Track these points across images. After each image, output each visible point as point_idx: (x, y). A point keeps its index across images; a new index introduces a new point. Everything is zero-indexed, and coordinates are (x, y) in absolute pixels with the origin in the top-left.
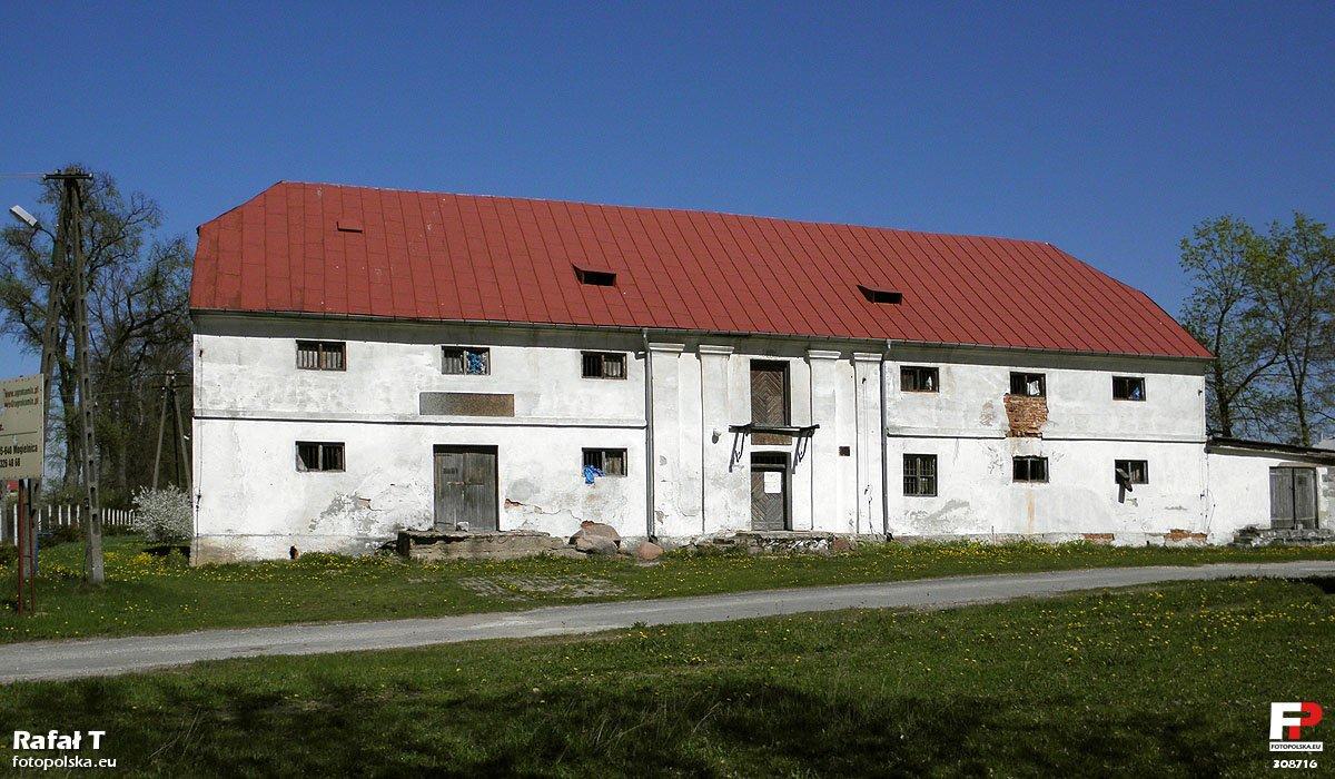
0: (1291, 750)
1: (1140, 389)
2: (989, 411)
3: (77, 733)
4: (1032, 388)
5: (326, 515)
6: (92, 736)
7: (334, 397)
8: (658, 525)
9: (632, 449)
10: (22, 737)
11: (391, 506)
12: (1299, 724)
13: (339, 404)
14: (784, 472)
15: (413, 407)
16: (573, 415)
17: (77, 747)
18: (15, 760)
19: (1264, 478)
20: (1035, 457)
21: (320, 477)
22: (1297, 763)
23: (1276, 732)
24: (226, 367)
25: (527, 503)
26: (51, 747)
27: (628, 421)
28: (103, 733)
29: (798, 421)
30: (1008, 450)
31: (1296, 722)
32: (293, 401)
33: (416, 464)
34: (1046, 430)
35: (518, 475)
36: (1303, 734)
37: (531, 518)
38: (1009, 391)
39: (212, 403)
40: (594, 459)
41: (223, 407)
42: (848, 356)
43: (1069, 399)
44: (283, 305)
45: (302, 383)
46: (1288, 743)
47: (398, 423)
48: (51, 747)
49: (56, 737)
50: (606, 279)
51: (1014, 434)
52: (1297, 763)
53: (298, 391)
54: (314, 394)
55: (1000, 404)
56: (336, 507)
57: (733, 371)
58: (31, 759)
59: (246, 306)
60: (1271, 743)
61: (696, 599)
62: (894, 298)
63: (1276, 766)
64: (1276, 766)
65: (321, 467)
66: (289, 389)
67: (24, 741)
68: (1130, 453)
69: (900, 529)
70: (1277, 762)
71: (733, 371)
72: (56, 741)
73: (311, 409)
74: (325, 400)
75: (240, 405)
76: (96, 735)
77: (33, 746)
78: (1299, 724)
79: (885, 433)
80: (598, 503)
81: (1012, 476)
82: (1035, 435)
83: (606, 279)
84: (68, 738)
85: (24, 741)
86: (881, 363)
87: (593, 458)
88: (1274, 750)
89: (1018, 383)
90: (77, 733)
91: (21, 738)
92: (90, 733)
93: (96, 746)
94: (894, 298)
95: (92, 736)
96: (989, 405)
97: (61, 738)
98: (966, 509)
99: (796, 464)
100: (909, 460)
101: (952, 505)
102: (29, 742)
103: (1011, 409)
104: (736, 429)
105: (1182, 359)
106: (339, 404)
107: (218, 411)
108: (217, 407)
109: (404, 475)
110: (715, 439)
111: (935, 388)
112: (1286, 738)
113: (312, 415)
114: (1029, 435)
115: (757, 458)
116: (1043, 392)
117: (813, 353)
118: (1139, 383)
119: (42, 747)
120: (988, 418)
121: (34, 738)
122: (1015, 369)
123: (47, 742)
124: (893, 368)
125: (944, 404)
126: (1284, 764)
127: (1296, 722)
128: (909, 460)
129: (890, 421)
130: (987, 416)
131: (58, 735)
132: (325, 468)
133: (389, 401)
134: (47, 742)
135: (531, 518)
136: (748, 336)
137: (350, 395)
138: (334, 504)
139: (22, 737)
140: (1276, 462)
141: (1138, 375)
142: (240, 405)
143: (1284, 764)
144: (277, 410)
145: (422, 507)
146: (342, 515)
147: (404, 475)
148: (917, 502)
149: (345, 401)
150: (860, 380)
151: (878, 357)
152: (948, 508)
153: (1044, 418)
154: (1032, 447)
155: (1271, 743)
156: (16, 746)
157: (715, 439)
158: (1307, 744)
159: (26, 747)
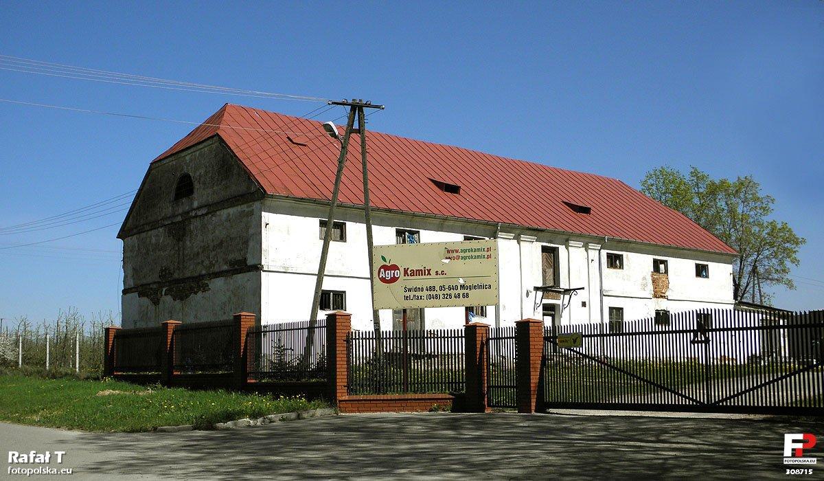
0: (797, 463)
1: (706, 272)
3: (47, 453)
4: (662, 267)
6: (57, 455)
10: (13, 455)
12: (802, 447)
14: (553, 317)
17: (47, 461)
18: (9, 469)
20: (664, 310)
22: (800, 471)
23: (787, 452)
26: (32, 461)
28: (64, 453)
29: (564, 285)
31: (800, 446)
34: (669, 294)
36: (805, 453)
42: (518, 238)
46: (795, 459)
48: (32, 461)
49: (34, 455)
50: (454, 189)
51: (655, 296)
52: (800, 471)
57: (532, 250)
58: (19, 469)
60: (785, 459)
62: (586, 210)
63: (788, 473)
64: (788, 473)
65: (332, 308)
67: (15, 458)
70: (788, 470)
71: (532, 250)
72: (35, 457)
76: (60, 453)
77: (37, 460)
78: (802, 447)
79: (602, 295)
83: (454, 189)
84: (42, 456)
85: (15, 458)
86: (600, 251)
88: (786, 463)
89: (656, 263)
90: (47, 453)
91: (12, 456)
92: (56, 453)
93: (59, 461)
94: (586, 210)
95: (57, 455)
97: (38, 455)
99: (562, 312)
102: (18, 458)
104: (537, 289)
105: (670, 247)
110: (527, 295)
111: (621, 267)
112: (793, 455)
114: (662, 297)
116: (666, 272)
117: (571, 243)
118: (620, 257)
119: (26, 461)
121: (21, 455)
122: (545, 244)
123: (29, 458)
124: (604, 253)
126: (793, 472)
127: (800, 446)
128: (611, 309)
131: (36, 454)
134: (29, 458)
136: (542, 231)
139: (13, 455)
141: (620, 253)
143: (793, 472)
150: (590, 261)
151: (599, 247)
155: (785, 459)
156: (10, 461)
157: (527, 295)
158: (806, 459)
159: (16, 461)
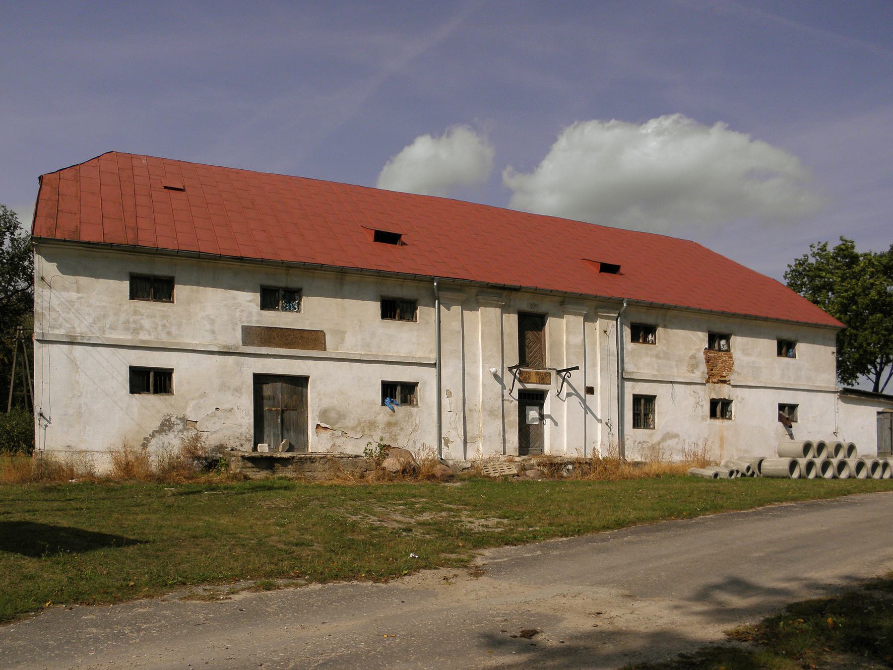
2: (693, 362)
5: (157, 435)
7: (164, 326)
8: (445, 450)
9: (703, 419)
11: (217, 427)
13: (169, 333)
15: (235, 339)
16: (375, 352)
19: (875, 417)
20: (725, 399)
21: (151, 401)
24: (66, 295)
25: (335, 427)
27: (824, 387)
30: (705, 395)
32: (127, 329)
33: (238, 390)
34: (734, 379)
35: (326, 403)
37: (339, 442)
38: (707, 346)
39: (53, 327)
40: (389, 390)
41: (62, 331)
43: (749, 354)
44: (119, 238)
45: (136, 312)
47: (464, 396)
53: (131, 320)
54: (146, 323)
55: (701, 356)
56: (166, 426)
59: (85, 238)
61: (309, 435)
66: (123, 317)
68: (788, 398)
69: (633, 455)
73: (144, 337)
74: (156, 328)
75: (78, 330)
80: (395, 429)
81: (709, 414)
82: (725, 382)
87: (389, 390)
89: (713, 338)
96: (693, 357)
98: (677, 440)
100: (637, 399)
101: (667, 436)
103: (708, 361)
106: (169, 333)
107: (57, 335)
108: (57, 332)
109: (227, 400)
113: (144, 342)
115: (525, 394)
120: (693, 367)
125: (662, 355)
128: (637, 399)
129: (629, 367)
130: (693, 365)
132: (156, 392)
133: (213, 332)
135: (339, 442)
137: (180, 325)
138: (163, 424)
140: (881, 409)
142: (78, 330)
144: (112, 336)
145: (244, 430)
146: (171, 435)
147: (227, 400)
148: (641, 433)
149: (174, 330)
152: (664, 439)
153: (730, 369)
154: (724, 392)
